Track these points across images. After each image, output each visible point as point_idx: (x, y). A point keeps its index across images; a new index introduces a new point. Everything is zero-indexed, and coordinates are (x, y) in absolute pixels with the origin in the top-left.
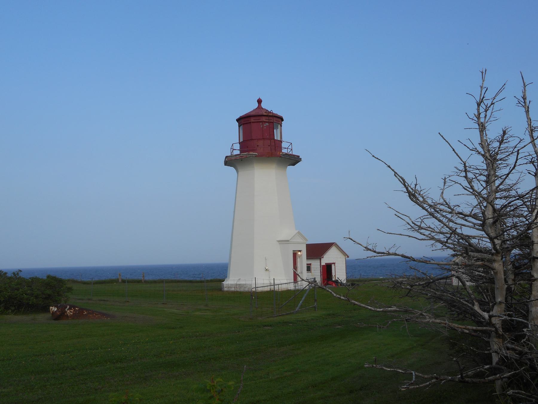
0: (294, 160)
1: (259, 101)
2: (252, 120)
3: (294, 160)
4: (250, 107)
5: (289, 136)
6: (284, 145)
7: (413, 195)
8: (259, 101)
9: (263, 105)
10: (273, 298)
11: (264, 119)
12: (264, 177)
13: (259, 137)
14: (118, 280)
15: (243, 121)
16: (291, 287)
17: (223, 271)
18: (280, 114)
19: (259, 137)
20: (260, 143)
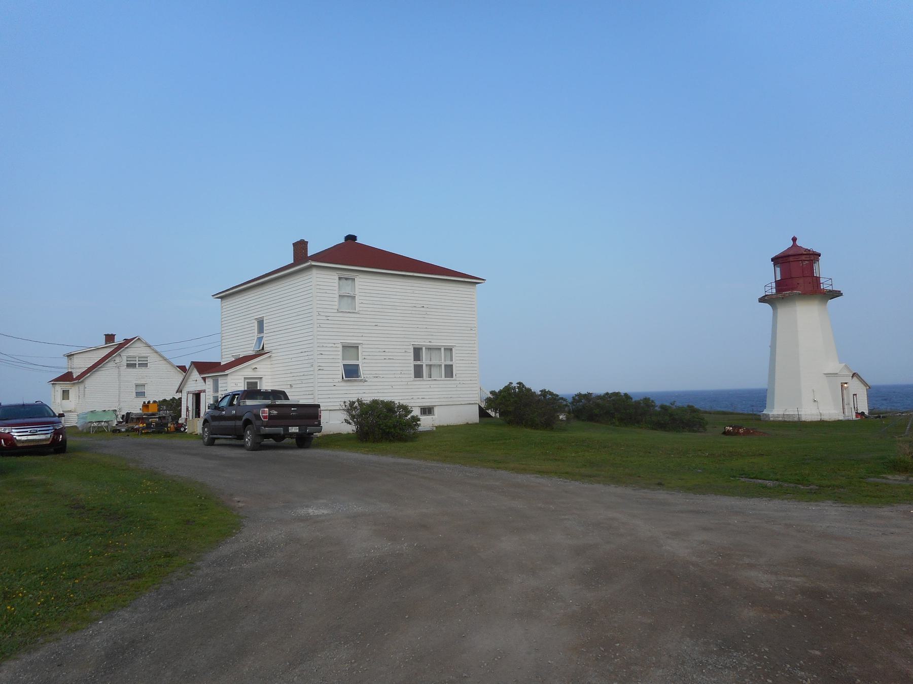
0: (836, 294)
1: (794, 239)
2: (791, 259)
3: (836, 294)
4: (782, 246)
5: (827, 272)
6: (822, 280)
7: (127, 341)
8: (794, 239)
9: (798, 243)
10: (821, 426)
11: (803, 258)
12: (805, 315)
13: (797, 275)
14: (310, 413)
15: (777, 260)
16: (841, 418)
17: (761, 398)
18: (818, 251)
19: (797, 275)
20: (801, 281)
